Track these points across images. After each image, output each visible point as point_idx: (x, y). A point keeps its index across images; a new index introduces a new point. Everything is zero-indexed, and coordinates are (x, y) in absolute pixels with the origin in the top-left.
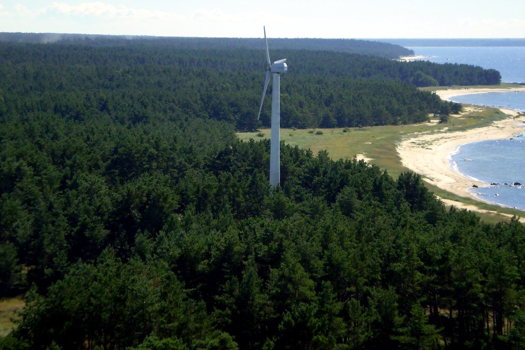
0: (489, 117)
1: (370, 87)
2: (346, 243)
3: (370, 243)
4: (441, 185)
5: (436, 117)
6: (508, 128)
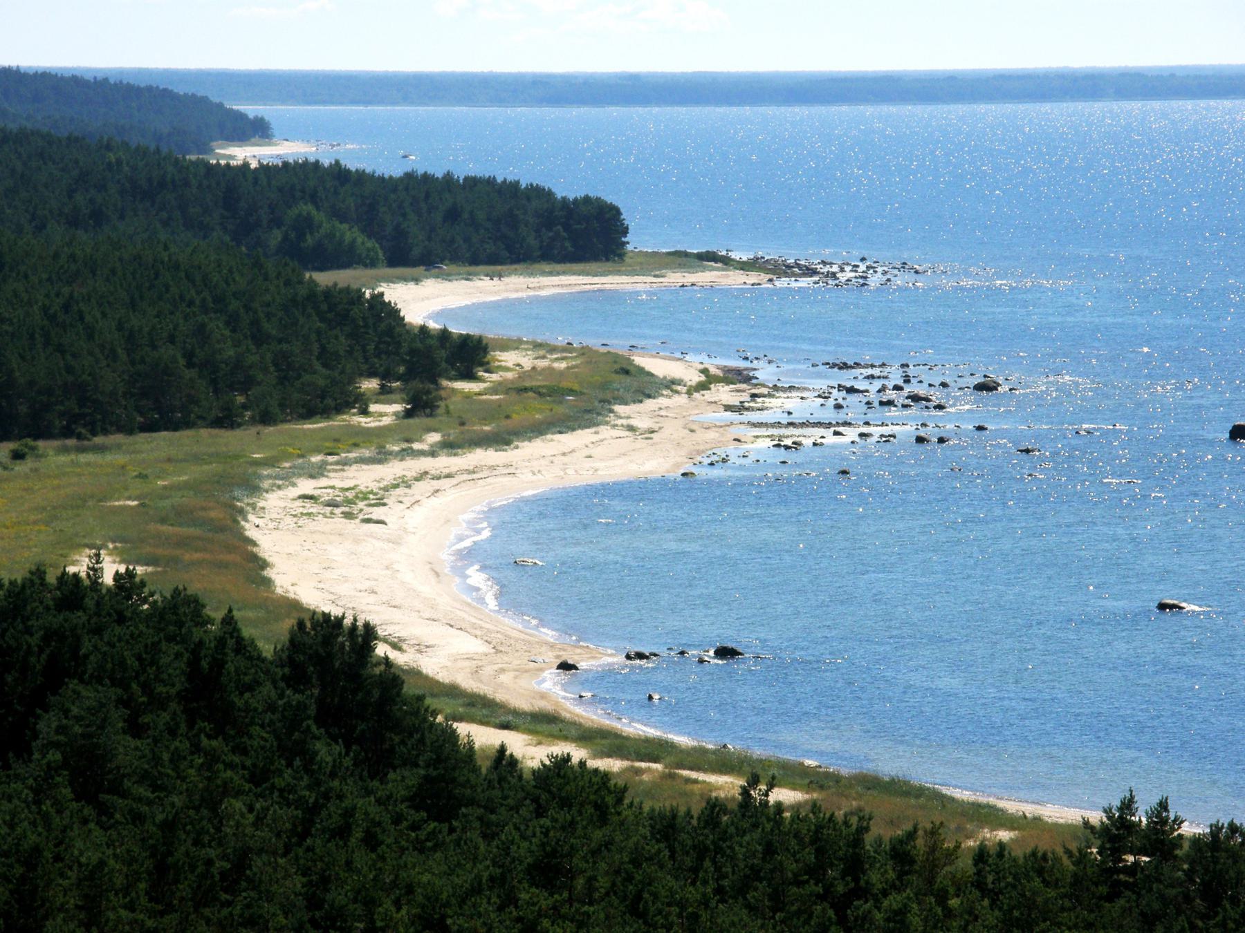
0: (595, 389)
1: (113, 272)
2: (111, 915)
3: (207, 912)
4: (435, 666)
5: (391, 391)
6: (672, 430)
